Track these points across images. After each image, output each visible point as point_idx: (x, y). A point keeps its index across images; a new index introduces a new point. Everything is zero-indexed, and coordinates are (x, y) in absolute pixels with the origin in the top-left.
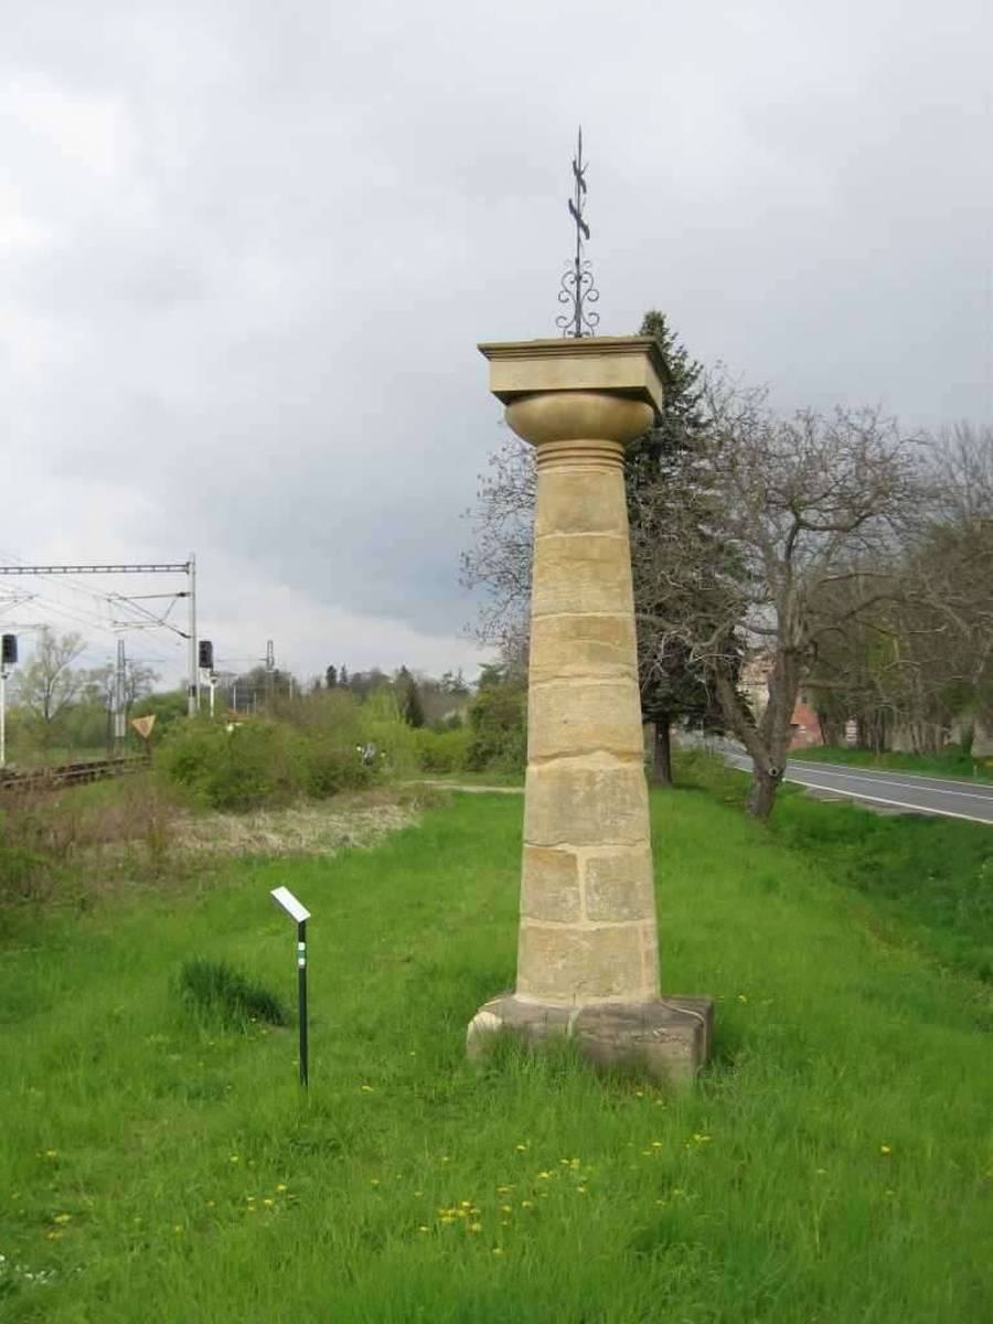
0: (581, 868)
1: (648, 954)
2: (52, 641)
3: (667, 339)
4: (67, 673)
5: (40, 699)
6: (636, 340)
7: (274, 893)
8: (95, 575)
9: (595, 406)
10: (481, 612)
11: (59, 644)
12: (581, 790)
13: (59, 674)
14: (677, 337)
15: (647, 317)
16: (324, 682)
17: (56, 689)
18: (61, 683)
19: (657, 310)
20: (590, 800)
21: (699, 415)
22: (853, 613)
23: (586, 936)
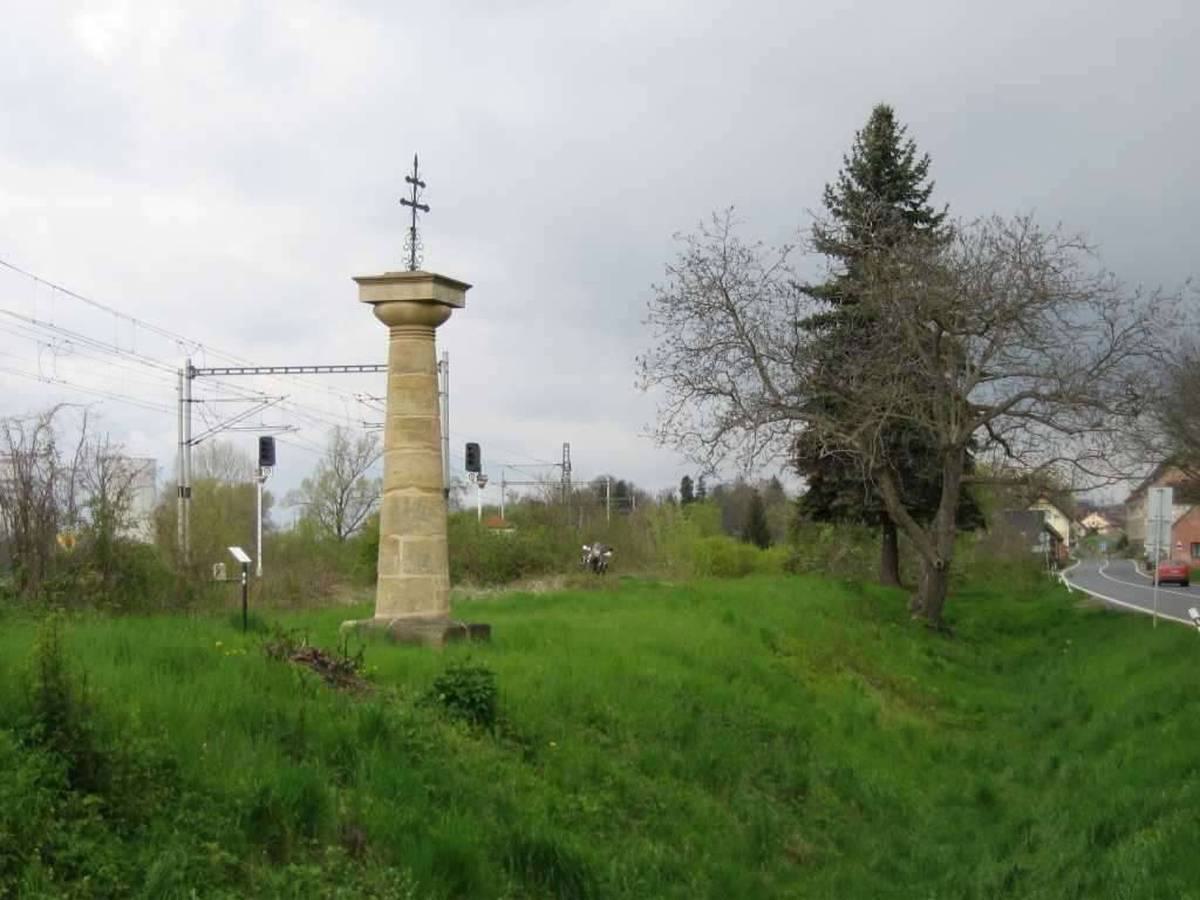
0: (401, 545)
1: (438, 593)
2: (345, 447)
3: (896, 133)
4: (362, 483)
5: (332, 513)
6: (407, 276)
7: (231, 549)
8: (331, 374)
9: (409, 309)
10: (659, 412)
11: (353, 449)
12: (402, 506)
13: (354, 484)
14: (906, 131)
15: (876, 111)
16: (678, 496)
17: (350, 502)
18: (356, 494)
19: (885, 104)
20: (407, 511)
21: (930, 211)
22: (773, 406)
23: (402, 581)
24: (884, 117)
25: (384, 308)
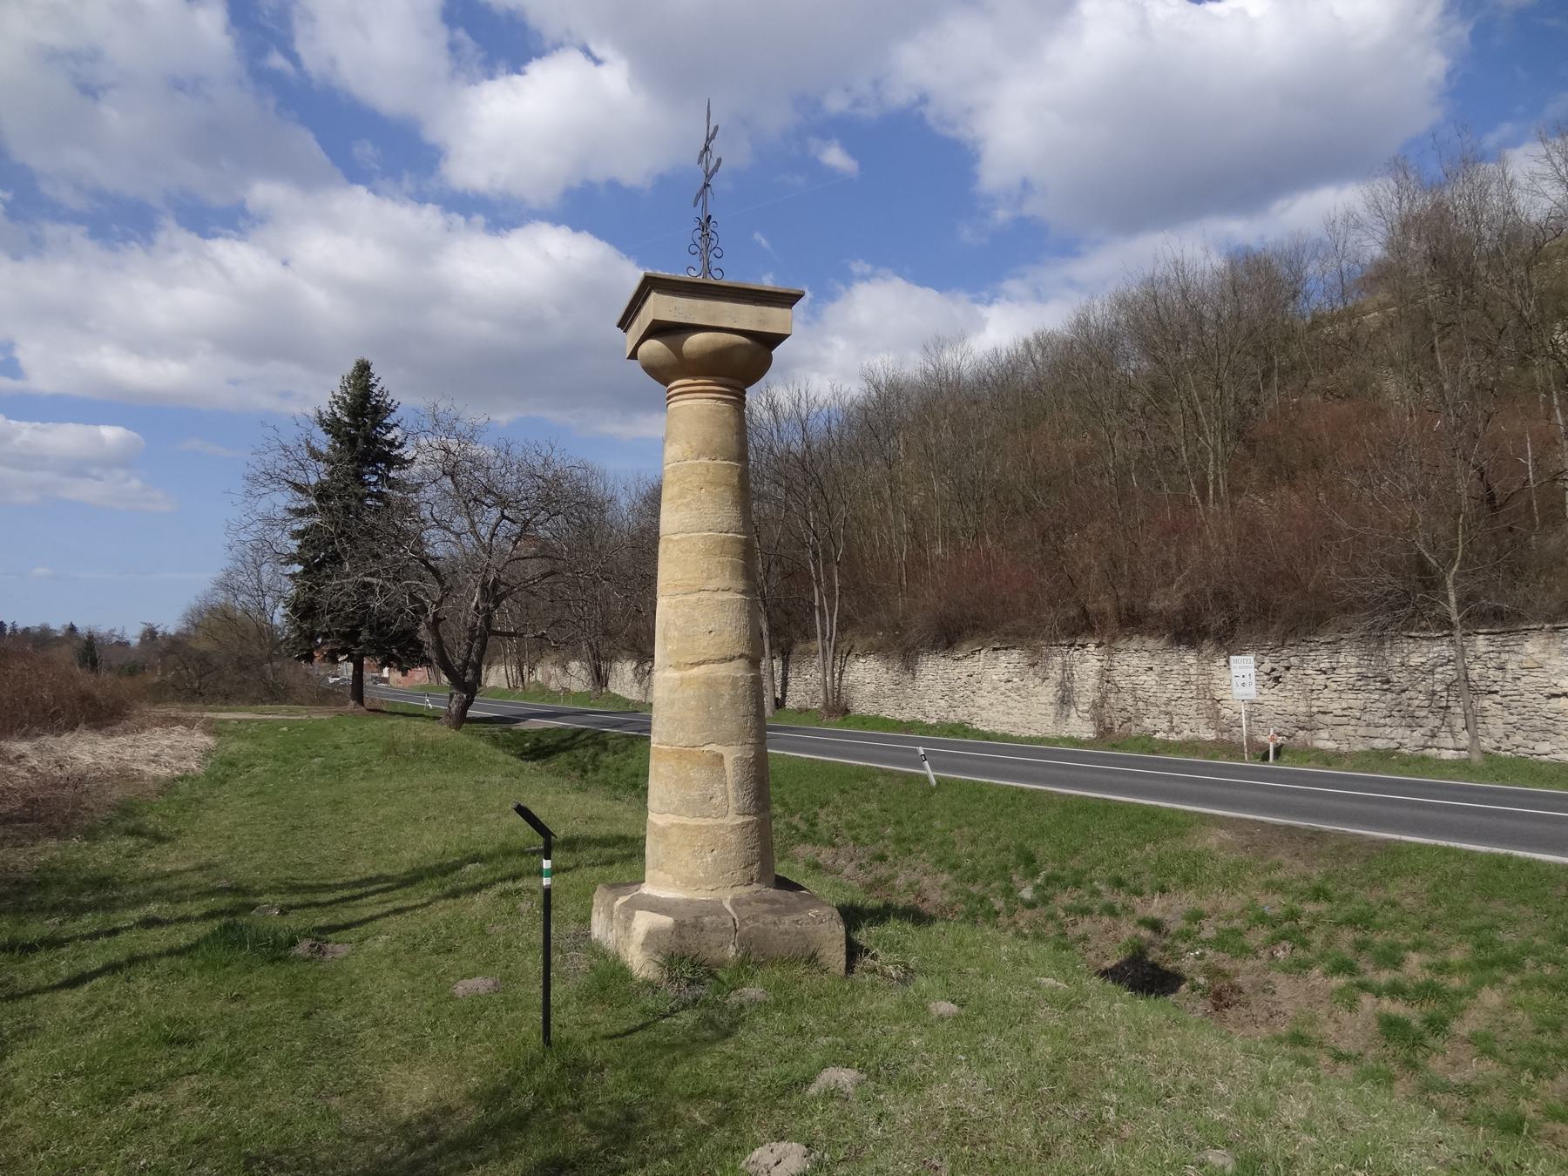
3: (372, 381)
24: (363, 369)
25: (695, 342)
